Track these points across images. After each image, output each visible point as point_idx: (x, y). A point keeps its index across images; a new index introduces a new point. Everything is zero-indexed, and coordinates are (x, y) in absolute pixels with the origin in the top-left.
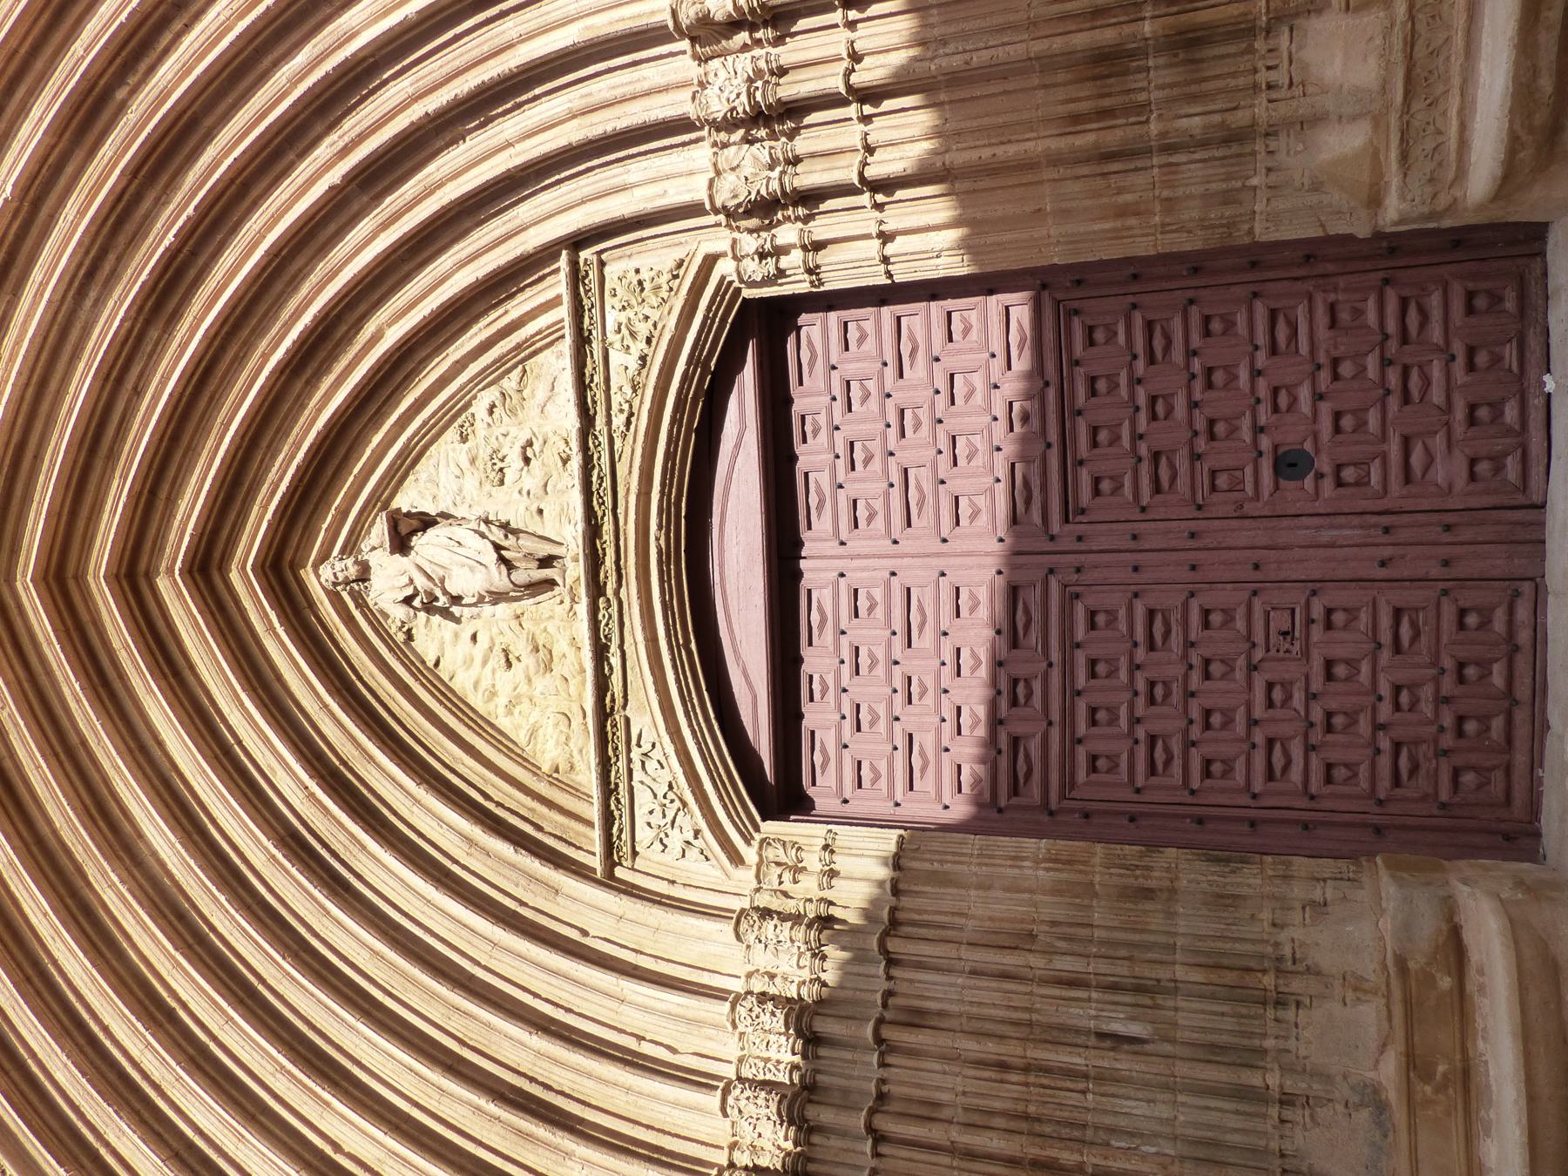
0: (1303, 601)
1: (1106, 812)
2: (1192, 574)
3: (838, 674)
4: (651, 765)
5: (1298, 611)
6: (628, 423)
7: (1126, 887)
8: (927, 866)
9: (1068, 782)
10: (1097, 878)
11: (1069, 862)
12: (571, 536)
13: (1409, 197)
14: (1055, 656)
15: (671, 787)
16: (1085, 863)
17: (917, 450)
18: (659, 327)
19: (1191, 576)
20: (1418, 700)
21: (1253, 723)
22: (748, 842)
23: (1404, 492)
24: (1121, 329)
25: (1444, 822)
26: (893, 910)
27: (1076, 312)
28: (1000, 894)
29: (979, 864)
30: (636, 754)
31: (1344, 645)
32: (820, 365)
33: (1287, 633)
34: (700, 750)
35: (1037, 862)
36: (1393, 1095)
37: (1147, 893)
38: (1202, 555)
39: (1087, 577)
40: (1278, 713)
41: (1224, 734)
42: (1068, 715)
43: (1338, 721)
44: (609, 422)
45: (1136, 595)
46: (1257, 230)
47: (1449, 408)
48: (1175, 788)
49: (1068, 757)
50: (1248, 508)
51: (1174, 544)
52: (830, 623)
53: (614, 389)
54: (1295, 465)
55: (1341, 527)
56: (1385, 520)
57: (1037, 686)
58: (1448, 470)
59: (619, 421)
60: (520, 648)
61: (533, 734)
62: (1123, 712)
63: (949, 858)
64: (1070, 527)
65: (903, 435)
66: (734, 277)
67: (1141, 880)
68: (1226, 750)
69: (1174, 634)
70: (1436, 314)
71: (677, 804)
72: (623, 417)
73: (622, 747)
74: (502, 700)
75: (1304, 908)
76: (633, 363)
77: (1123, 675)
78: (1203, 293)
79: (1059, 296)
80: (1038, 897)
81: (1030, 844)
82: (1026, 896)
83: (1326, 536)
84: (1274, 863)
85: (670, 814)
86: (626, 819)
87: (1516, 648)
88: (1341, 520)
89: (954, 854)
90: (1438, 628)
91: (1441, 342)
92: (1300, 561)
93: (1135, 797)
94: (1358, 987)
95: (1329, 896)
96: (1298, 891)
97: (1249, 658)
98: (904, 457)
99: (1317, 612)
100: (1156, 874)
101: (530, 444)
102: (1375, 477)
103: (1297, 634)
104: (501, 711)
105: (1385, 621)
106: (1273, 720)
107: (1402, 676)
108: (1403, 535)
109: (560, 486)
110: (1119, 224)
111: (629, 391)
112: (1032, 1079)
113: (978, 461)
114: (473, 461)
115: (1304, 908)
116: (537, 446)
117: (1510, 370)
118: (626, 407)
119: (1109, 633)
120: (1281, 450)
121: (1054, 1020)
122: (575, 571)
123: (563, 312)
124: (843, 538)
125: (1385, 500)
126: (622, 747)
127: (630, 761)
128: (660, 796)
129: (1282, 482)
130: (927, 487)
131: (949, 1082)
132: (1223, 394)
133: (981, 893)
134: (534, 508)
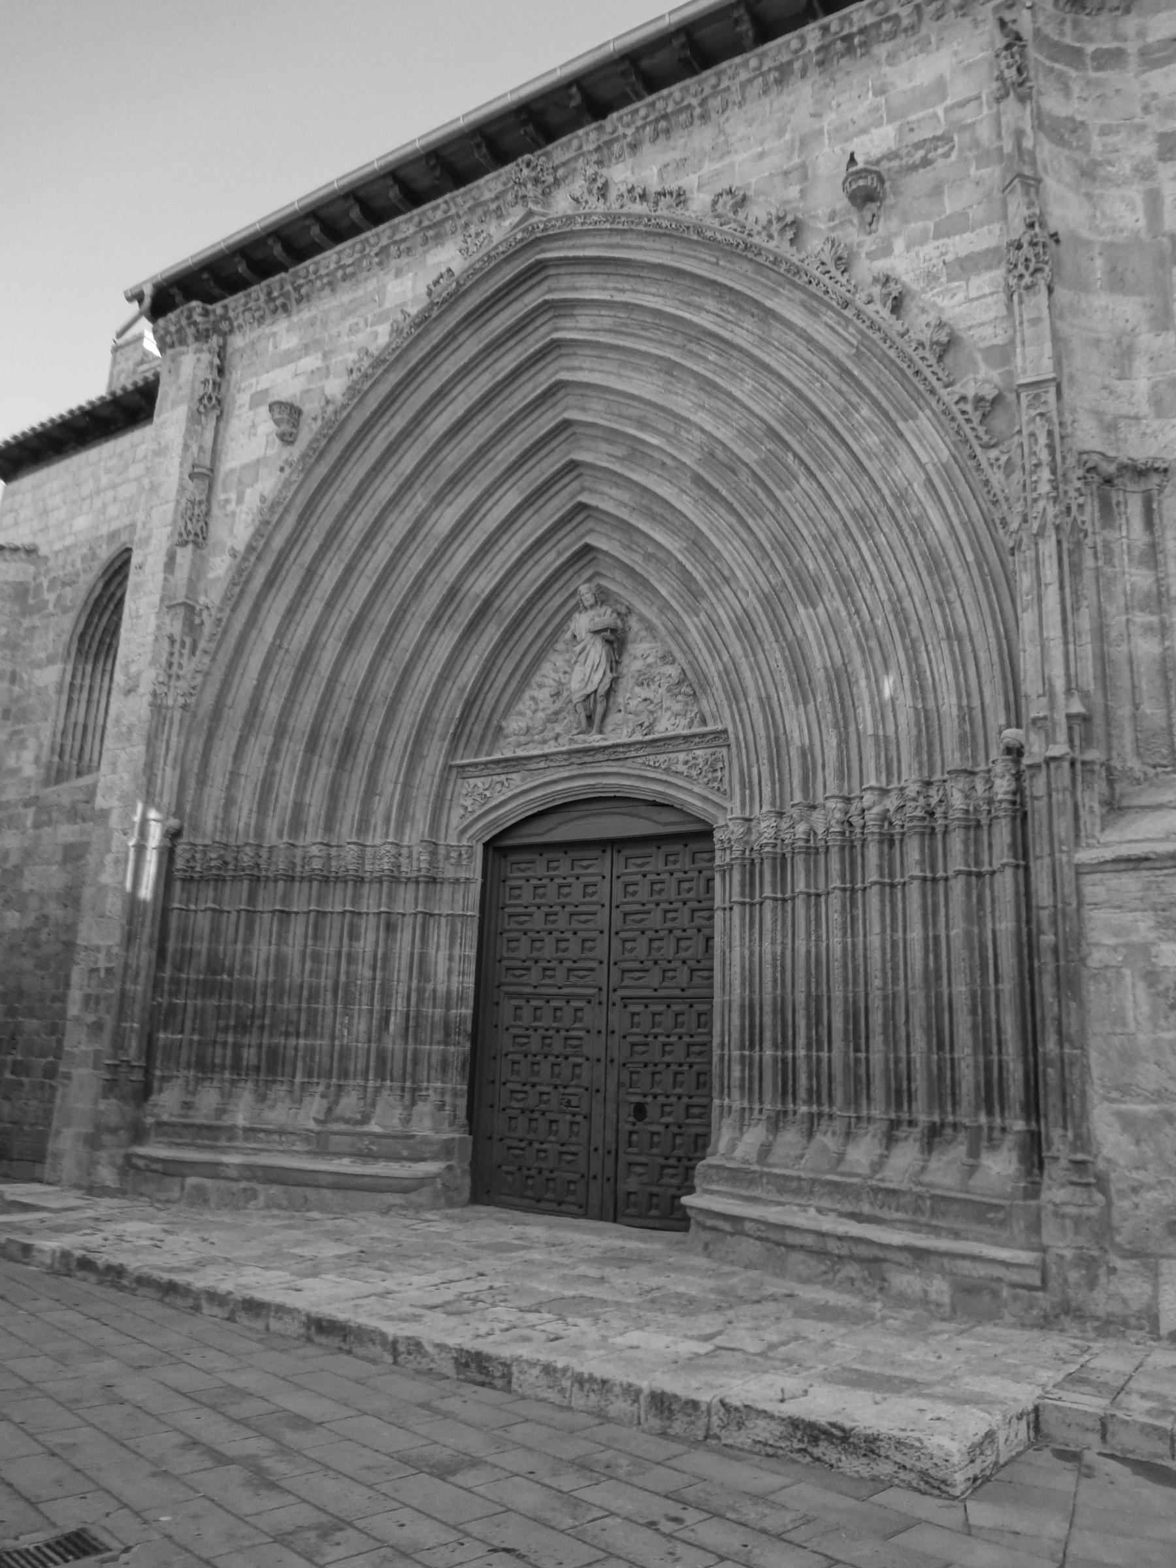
21: (534, 1086)
30: (503, 777)
31: (564, 1129)
36: (366, 1128)
42: (538, 996)
49: (520, 995)
61: (521, 714)
81: (470, 982)
87: (560, 1204)
94: (407, 1121)
96: (448, 1099)
105: (573, 1149)
114: (649, 665)
122: (595, 739)
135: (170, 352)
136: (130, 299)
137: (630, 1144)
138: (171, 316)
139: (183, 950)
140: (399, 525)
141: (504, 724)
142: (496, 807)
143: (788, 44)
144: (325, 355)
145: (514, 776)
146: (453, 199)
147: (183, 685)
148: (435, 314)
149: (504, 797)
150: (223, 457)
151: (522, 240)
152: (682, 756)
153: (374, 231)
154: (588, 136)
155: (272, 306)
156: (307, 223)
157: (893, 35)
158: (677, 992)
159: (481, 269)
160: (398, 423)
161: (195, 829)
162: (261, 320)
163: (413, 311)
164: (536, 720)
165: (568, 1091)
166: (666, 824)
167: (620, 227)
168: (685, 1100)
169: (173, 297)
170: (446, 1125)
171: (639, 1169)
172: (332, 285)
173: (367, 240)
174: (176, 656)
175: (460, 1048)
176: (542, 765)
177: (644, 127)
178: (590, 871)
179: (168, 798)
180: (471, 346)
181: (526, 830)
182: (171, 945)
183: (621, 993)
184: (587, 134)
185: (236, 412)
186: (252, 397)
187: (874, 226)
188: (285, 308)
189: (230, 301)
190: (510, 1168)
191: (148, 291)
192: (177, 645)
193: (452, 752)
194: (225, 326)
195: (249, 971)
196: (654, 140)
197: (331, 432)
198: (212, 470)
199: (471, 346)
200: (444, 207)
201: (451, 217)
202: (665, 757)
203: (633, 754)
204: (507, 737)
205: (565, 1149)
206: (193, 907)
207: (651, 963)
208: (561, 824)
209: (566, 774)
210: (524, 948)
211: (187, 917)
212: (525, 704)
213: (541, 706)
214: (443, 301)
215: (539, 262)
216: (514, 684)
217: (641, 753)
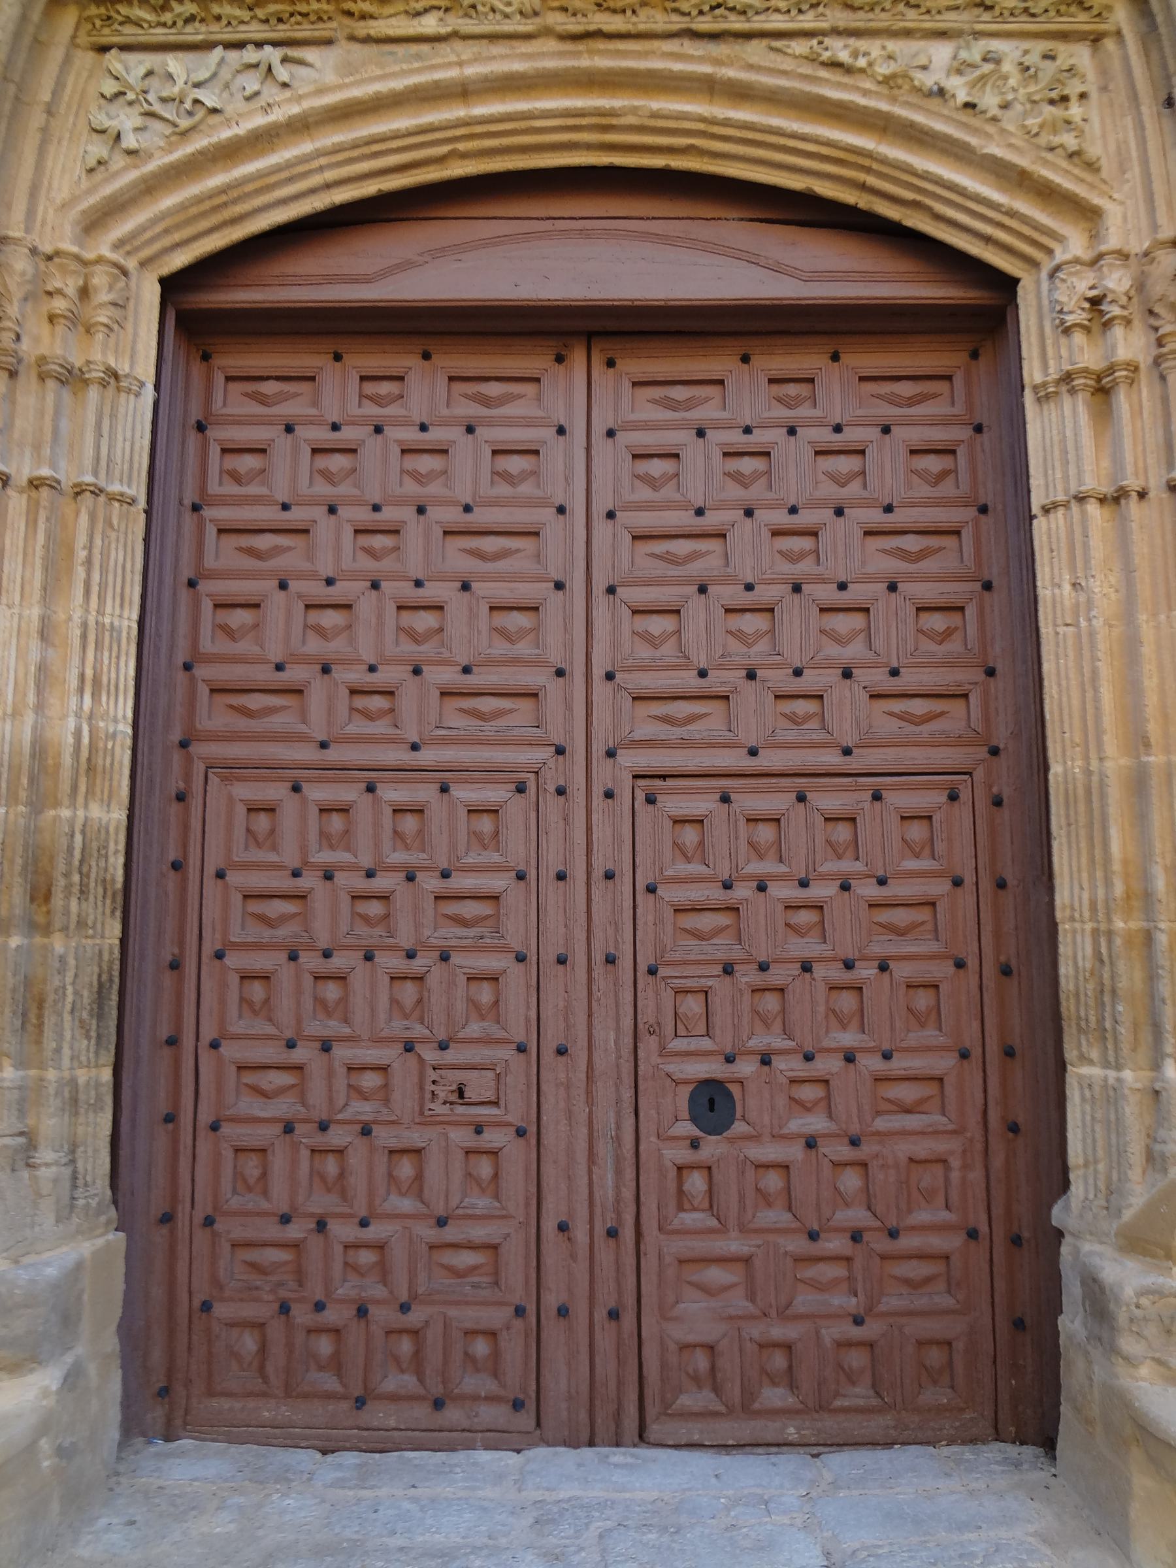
0: (509, 1118)
1: (186, 827)
2: (552, 958)
3: (404, 422)
4: (251, 81)
5: (494, 1111)
6: (835, 65)
7: (52, 859)
8: (82, 539)
9: (232, 770)
10: (65, 813)
11: (91, 769)
13: (1144, 1301)
14: (427, 756)
15: (215, 111)
16: (90, 792)
17: (752, 554)
18: (990, 129)
19: (549, 956)
20: (362, 1275)
22: (118, 245)
23: (668, 1259)
24: (925, 864)
25: (182, 1311)
27: (953, 797)
28: (34, 656)
29: (85, 625)
30: (272, 54)
32: (889, 412)
33: (461, 1094)
34: (278, 169)
37: (41, 894)
38: (581, 974)
39: (552, 804)
40: (341, 1083)
41: (308, 1003)
43: (331, 1166)
44: (836, 32)
45: (521, 877)
46: (1085, 1070)
47: (785, 1314)
48: (225, 932)
50: (649, 1045)
51: (598, 933)
52: (484, 411)
53: (892, 45)
54: (712, 1109)
55: (618, 1172)
56: (628, 1233)
57: (381, 727)
58: (696, 1318)
59: (840, 49)
62: (344, 857)
63: (96, 577)
64: (628, 781)
65: (776, 533)
66: (1060, 256)
67: (62, 882)
68: (285, 1007)
69: (460, 931)
70: (921, 1302)
71: (184, 123)
72: (844, 56)
75: (22, 1134)
77: (398, 857)
78: (974, 981)
79: (979, 774)
80: (29, 718)
81: (121, 710)
82: (31, 698)
83: (605, 1150)
84: (98, 1085)
85: (167, 112)
86: (160, 35)
88: (629, 1174)
89: (103, 586)
90: (467, 1303)
91: (882, 1308)
92: (570, 1114)
93: (210, 870)
95: (44, 1172)
96: (50, 1124)
97: (423, 1041)
98: (743, 532)
99: (493, 1138)
100: (74, 905)
102: (690, 1219)
103: (460, 1110)
105: (479, 1233)
106: (330, 1074)
107: (398, 1255)
108: (605, 1257)
110: (1117, 866)
111: (883, 69)
113: (734, 645)
115: (22, 1134)
117: (837, 1394)
118: (862, 62)
119: (462, 837)
120: (734, 1089)
124: (620, 436)
125: (655, 1232)
127: (259, 45)
128: (200, 94)
129: (685, 1092)
130: (696, 569)
132: (822, 1009)
133: (35, 624)
137: (682, 1200)
142: (231, 152)
145: (310, 54)
158: (832, 759)
165: (450, 1056)
168: (871, 1063)
170: (47, 1219)
171: (716, 1275)
175: (86, 941)
183: (629, 760)
190: (249, 1311)
205: (451, 1233)
208: (440, 252)
210: (281, 628)
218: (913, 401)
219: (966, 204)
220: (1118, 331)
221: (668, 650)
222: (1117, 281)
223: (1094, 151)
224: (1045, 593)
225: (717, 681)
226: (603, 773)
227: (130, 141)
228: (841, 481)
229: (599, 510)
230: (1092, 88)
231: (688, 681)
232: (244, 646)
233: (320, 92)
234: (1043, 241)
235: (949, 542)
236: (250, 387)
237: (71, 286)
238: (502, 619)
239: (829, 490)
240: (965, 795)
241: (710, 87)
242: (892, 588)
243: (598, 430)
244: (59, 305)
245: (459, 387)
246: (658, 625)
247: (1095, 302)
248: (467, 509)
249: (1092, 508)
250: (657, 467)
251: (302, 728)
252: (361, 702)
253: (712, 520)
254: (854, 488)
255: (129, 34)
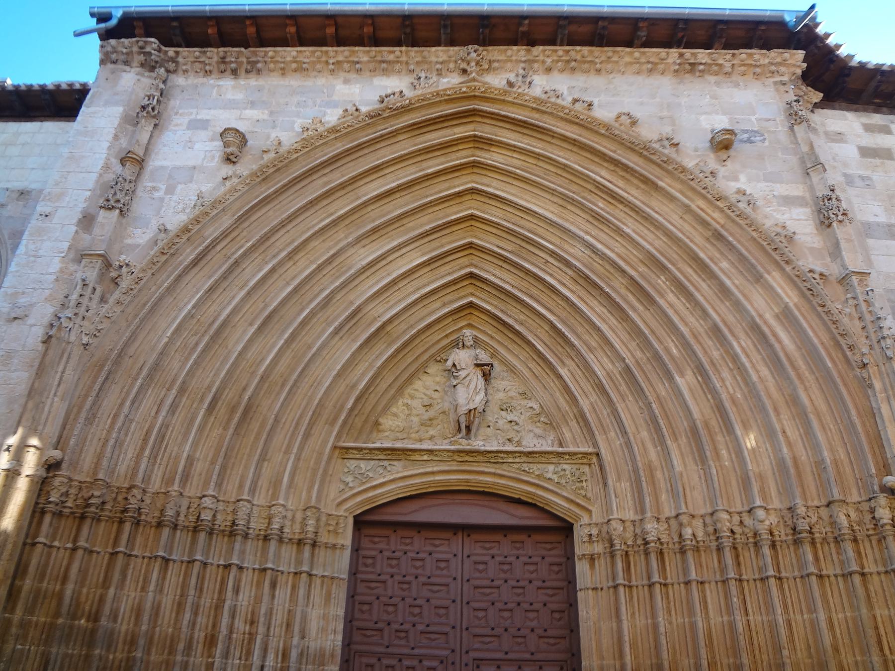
9: (362, 654)
12: (478, 444)
14: (416, 651)
26: (316, 575)
30: (386, 463)
32: (544, 553)
35: (333, 641)
49: (373, 653)
57: (403, 642)
60: (431, 413)
61: (395, 415)
65: (513, 587)
72: (527, 469)
73: (389, 457)
74: (409, 402)
76: (549, 475)
81: (340, 637)
86: (359, 456)
101: (517, 424)
104: (405, 401)
109: (499, 437)
111: (537, 473)
112: (247, 636)
114: (511, 398)
116: (516, 427)
121: (270, 647)
122: (464, 444)
123: (572, 449)
126: (389, 457)
131: (246, 599)
134: (491, 424)
135: (110, 66)
136: (92, 15)
138: (126, 41)
139: (38, 591)
140: (322, 251)
141: (381, 420)
143: (659, 53)
144: (271, 113)
145: (395, 463)
146: (407, 52)
147: (87, 326)
148: (386, 115)
149: (387, 481)
150: (153, 156)
151: (465, 92)
152: (551, 468)
153: (335, 48)
154: (518, 52)
155: (223, 67)
156: (288, 22)
157: (716, 74)
158: (527, 656)
159: (430, 99)
160: (338, 177)
161: (74, 465)
162: (208, 73)
163: (364, 109)
164: (399, 424)
166: (521, 518)
167: (544, 109)
169: (134, 28)
172: (283, 72)
173: (327, 52)
174: (86, 299)
176: (425, 457)
177: (558, 61)
178: (440, 549)
179: (52, 429)
180: (406, 146)
181: (389, 510)
182: (28, 584)
183: (473, 655)
184: (519, 51)
185: (171, 127)
186: (190, 122)
187: (726, 163)
188: (234, 72)
189: (184, 51)
191: (118, 14)
192: (90, 289)
193: (338, 436)
194: (172, 66)
195: (115, 620)
196: (562, 71)
197: (280, 165)
198: (143, 160)
199: (406, 146)
200: (398, 53)
201: (401, 62)
202: (539, 466)
203: (511, 460)
204: (383, 431)
206: (56, 543)
207: (502, 630)
208: (423, 508)
209: (447, 468)
211: (49, 555)
212: (398, 408)
213: (414, 412)
214: (389, 109)
215: (475, 110)
216: (392, 392)
217: (518, 460)
218: (550, 550)
219: (559, 504)
220: (596, 544)
221: (483, 621)
222: (594, 532)
223: (589, 495)
224: (580, 613)
225: (497, 631)
226: (465, 659)
227: (351, 485)
228: (519, 595)
229: (465, 579)
230: (589, 478)
231: (488, 631)
232: (366, 616)
233: (398, 473)
234: (579, 518)
235: (561, 591)
236: (370, 538)
237: (333, 523)
238: (438, 611)
239: (527, 575)
240: (565, 668)
241: (494, 474)
242: (545, 605)
243: (465, 556)
244: (331, 528)
245: (428, 541)
246: (481, 614)
247: (590, 535)
248: (429, 578)
249: (590, 592)
250: (481, 567)
251: (381, 641)
252: (399, 634)
253: (496, 583)
254: (534, 575)
255: (351, 456)
